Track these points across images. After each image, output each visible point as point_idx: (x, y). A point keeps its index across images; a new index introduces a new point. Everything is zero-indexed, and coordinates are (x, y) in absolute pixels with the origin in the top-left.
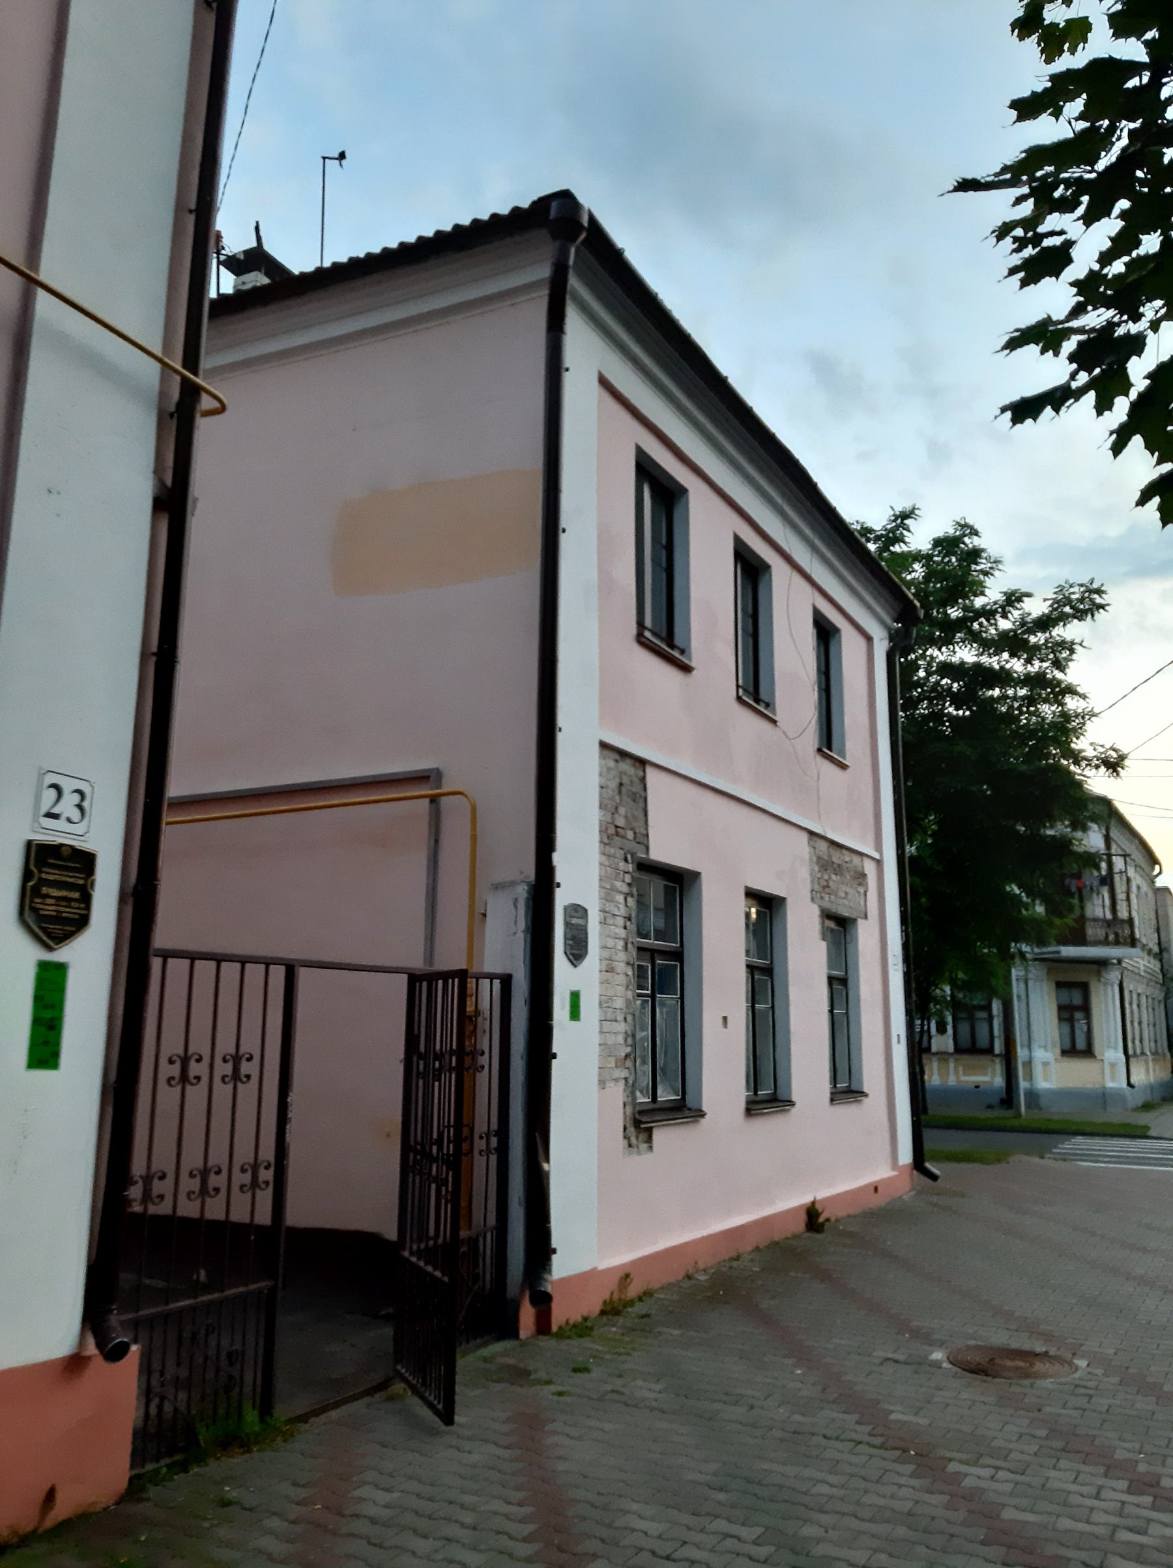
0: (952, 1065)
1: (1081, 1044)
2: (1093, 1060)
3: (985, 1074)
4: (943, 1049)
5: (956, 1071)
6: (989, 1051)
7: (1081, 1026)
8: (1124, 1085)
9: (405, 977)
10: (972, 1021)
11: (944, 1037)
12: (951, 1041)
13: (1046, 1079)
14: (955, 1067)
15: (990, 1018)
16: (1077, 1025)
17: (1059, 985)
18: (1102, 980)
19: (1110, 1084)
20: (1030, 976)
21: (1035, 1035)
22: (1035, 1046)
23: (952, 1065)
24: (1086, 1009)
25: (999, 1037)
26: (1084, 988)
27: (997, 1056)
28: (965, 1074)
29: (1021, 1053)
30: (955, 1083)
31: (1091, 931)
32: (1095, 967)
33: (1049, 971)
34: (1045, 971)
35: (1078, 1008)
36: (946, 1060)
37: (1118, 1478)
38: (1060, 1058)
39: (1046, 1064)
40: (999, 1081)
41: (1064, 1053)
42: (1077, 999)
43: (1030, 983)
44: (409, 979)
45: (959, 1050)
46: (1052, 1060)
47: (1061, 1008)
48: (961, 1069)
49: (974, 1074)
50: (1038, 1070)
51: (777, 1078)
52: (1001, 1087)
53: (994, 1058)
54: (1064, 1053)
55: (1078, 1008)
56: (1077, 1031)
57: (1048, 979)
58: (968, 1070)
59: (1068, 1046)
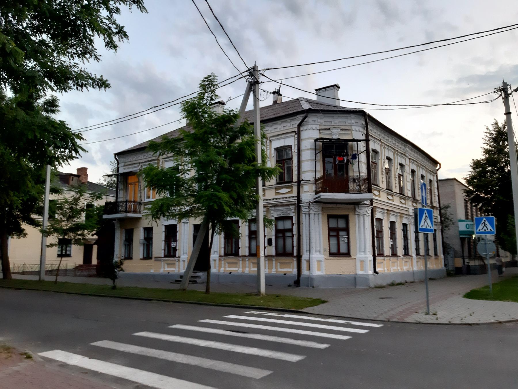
0: (274, 262)
1: (343, 249)
2: (348, 258)
3: (290, 268)
4: (270, 254)
5: (276, 266)
6: (291, 255)
7: (343, 240)
8: (371, 272)
9: (240, 254)
10: (284, 238)
11: (271, 247)
12: (274, 249)
13: (319, 270)
14: (276, 264)
15: (293, 236)
16: (341, 239)
17: (330, 217)
18: (356, 213)
19: (360, 272)
20: (311, 211)
21: (313, 245)
22: (313, 251)
23: (274, 262)
24: (347, 230)
25: (296, 246)
26: (346, 218)
27: (295, 257)
28: (281, 268)
29: (305, 256)
30: (275, 273)
31: (351, 186)
32: (352, 206)
33: (323, 209)
34: (320, 209)
35: (342, 230)
36: (272, 260)
37: (228, 270)
38: (329, 257)
39: (319, 261)
40: (295, 271)
41: (331, 254)
42: (342, 224)
43: (312, 216)
44: (239, 254)
45: (278, 254)
46: (323, 259)
47: (330, 230)
48: (279, 264)
49: (285, 268)
50: (314, 265)
51: (98, 297)
52: (295, 274)
53: (293, 258)
54: (331, 254)
55: (342, 230)
56: (341, 243)
57: (322, 214)
58: (282, 264)
59: (334, 250)
